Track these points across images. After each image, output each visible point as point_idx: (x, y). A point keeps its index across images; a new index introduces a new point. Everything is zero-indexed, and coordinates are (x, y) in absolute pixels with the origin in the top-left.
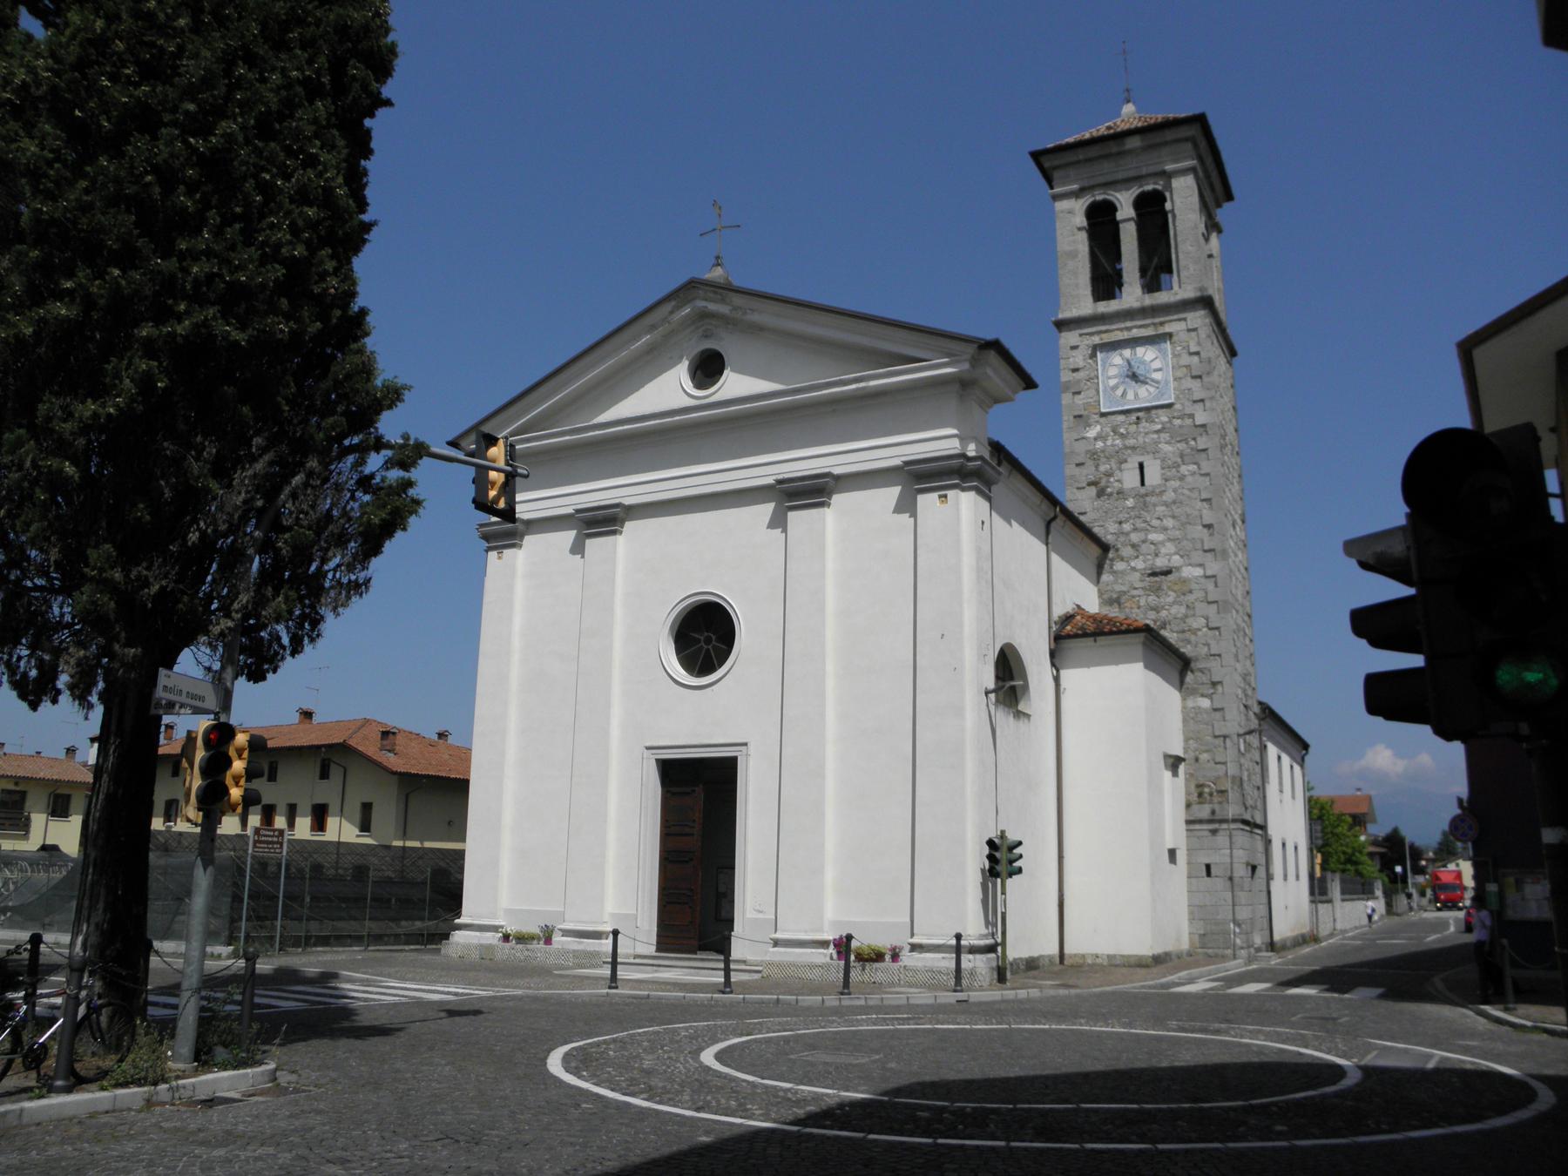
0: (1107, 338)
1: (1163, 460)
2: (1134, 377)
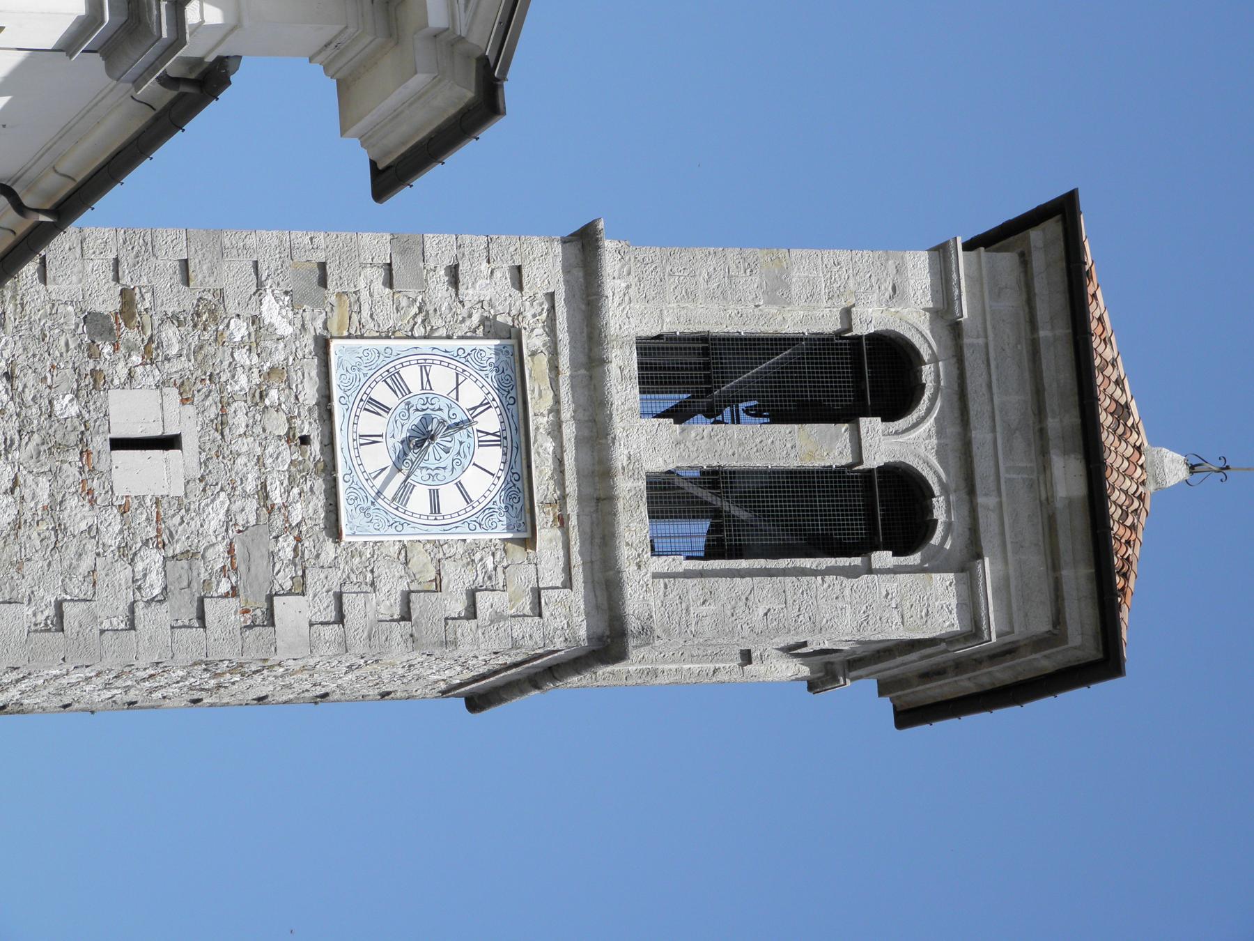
0: (537, 369)
1: (181, 504)
2: (422, 437)
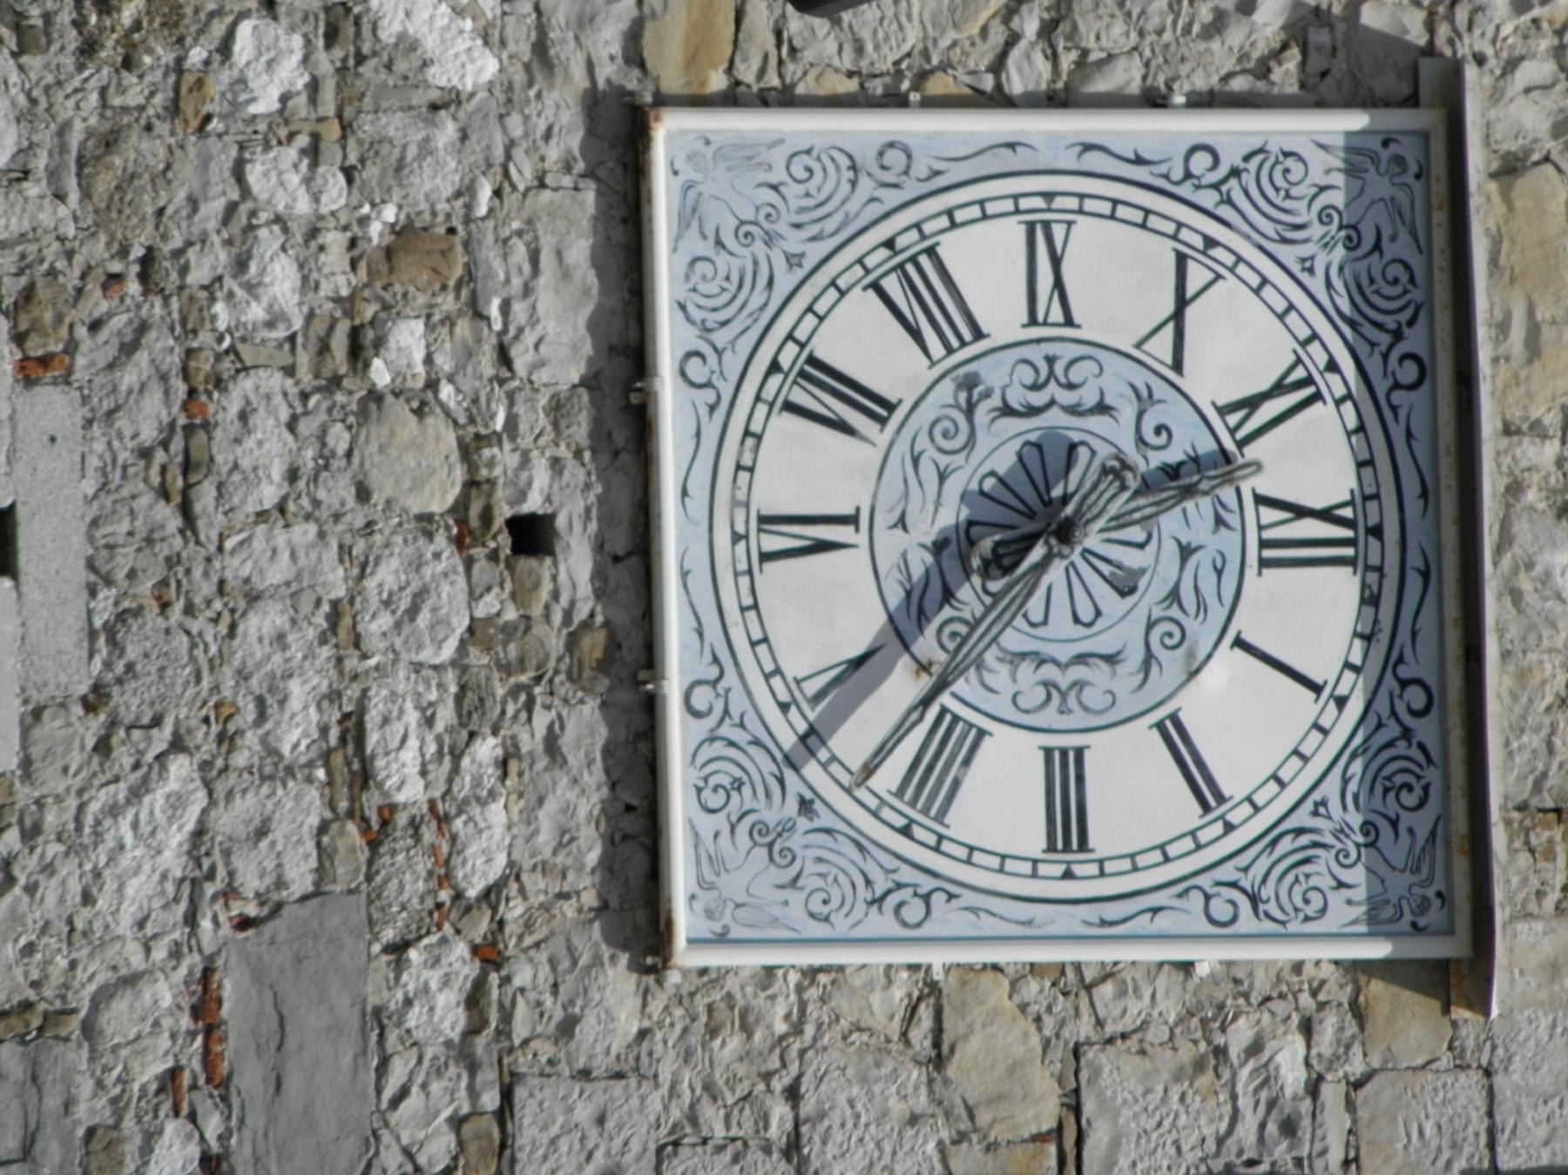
2: (1022, 526)
